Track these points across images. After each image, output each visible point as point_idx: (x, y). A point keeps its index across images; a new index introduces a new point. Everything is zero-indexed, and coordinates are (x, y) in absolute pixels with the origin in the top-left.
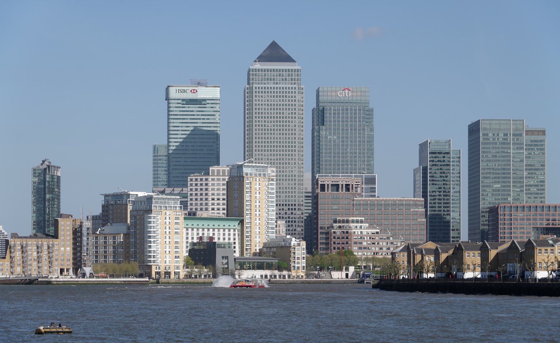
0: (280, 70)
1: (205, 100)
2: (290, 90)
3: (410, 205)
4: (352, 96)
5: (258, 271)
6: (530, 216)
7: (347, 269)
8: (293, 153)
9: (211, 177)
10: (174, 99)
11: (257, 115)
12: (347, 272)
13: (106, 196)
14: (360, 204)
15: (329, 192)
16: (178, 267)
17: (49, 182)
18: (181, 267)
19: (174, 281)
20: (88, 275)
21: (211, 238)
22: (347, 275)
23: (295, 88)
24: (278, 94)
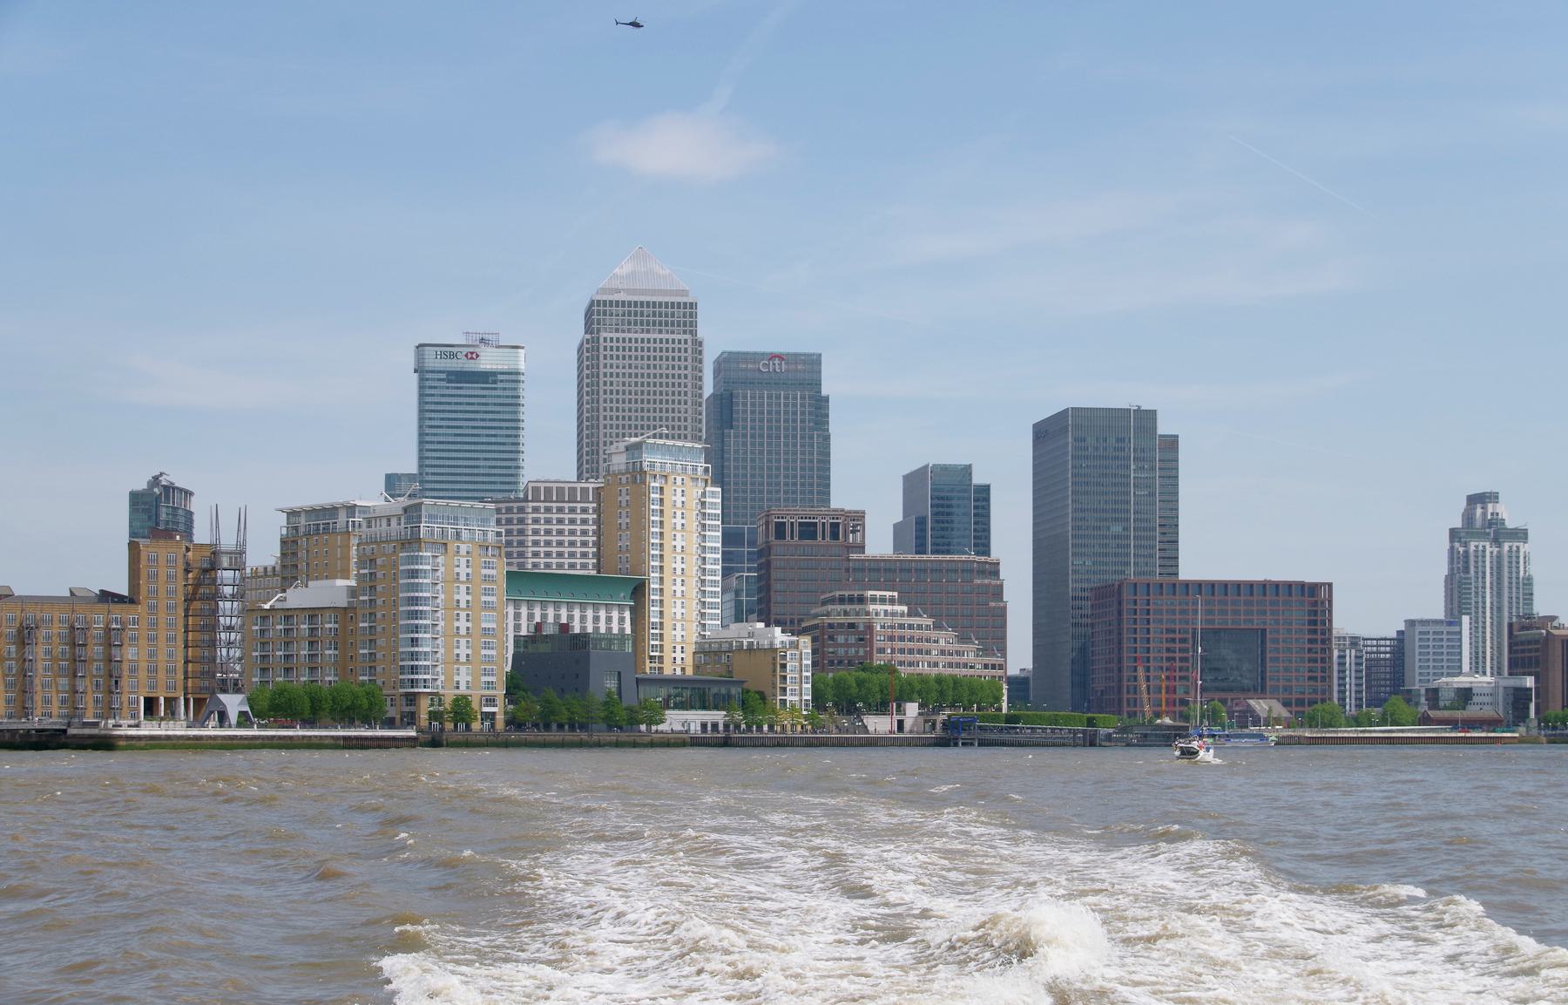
1: (494, 374)
3: (971, 571)
7: (900, 710)
13: (292, 514)
14: (863, 570)
16: (491, 701)
18: (500, 701)
19: (483, 739)
20: (233, 717)
21: (565, 628)
22: (901, 723)
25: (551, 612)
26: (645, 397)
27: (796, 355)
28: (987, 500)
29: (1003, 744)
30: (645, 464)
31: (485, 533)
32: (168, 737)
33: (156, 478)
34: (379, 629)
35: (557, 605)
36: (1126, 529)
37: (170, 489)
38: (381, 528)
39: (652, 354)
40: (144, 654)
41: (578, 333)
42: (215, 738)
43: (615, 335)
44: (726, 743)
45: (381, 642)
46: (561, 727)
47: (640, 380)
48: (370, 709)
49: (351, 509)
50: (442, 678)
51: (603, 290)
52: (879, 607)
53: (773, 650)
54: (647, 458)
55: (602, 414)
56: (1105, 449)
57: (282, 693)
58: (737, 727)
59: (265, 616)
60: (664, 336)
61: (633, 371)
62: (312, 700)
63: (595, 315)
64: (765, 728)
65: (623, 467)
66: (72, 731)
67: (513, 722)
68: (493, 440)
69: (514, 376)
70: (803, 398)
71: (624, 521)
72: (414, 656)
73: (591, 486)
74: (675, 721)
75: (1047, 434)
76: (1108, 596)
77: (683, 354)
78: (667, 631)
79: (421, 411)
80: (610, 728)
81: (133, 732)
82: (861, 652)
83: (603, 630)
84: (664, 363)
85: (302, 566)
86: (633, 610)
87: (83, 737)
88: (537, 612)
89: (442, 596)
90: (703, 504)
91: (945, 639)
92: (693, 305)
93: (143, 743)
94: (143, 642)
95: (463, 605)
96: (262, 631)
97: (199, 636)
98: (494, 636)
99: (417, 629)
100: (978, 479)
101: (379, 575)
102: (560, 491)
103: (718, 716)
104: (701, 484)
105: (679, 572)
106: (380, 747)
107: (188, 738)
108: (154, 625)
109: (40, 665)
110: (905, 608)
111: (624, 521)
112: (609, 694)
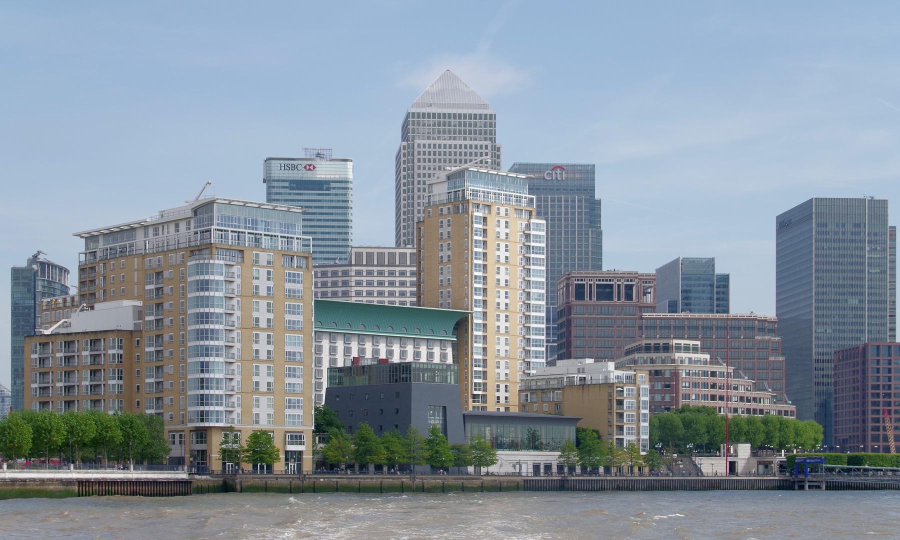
0: (465, 115)
1: (328, 182)
3: (753, 328)
4: (567, 179)
9: (354, 268)
10: (278, 181)
13: (91, 238)
15: (592, 301)
16: (297, 438)
18: (308, 438)
19: (285, 482)
22: (732, 467)
23: (486, 147)
25: (369, 346)
27: (574, 166)
28: (726, 286)
29: (866, 487)
30: (467, 193)
33: (35, 257)
34: (166, 353)
36: (861, 301)
41: (395, 142)
43: (427, 142)
44: (562, 486)
45: (169, 369)
46: (379, 468)
50: (238, 410)
51: (418, 105)
54: (470, 187)
56: (844, 233)
58: (572, 469)
60: (468, 142)
62: (38, 430)
64: (601, 470)
65: (444, 198)
67: (324, 464)
68: (327, 236)
70: (580, 201)
71: (445, 253)
73: (408, 251)
74: (508, 462)
75: (789, 224)
80: (434, 469)
82: (667, 398)
88: (354, 346)
89: (238, 313)
90: (528, 236)
95: (263, 324)
96: (42, 361)
99: (207, 351)
100: (719, 270)
101: (167, 290)
102: (381, 256)
103: (552, 457)
104: (525, 216)
105: (502, 307)
110: (708, 357)
111: (445, 253)
112: (434, 431)
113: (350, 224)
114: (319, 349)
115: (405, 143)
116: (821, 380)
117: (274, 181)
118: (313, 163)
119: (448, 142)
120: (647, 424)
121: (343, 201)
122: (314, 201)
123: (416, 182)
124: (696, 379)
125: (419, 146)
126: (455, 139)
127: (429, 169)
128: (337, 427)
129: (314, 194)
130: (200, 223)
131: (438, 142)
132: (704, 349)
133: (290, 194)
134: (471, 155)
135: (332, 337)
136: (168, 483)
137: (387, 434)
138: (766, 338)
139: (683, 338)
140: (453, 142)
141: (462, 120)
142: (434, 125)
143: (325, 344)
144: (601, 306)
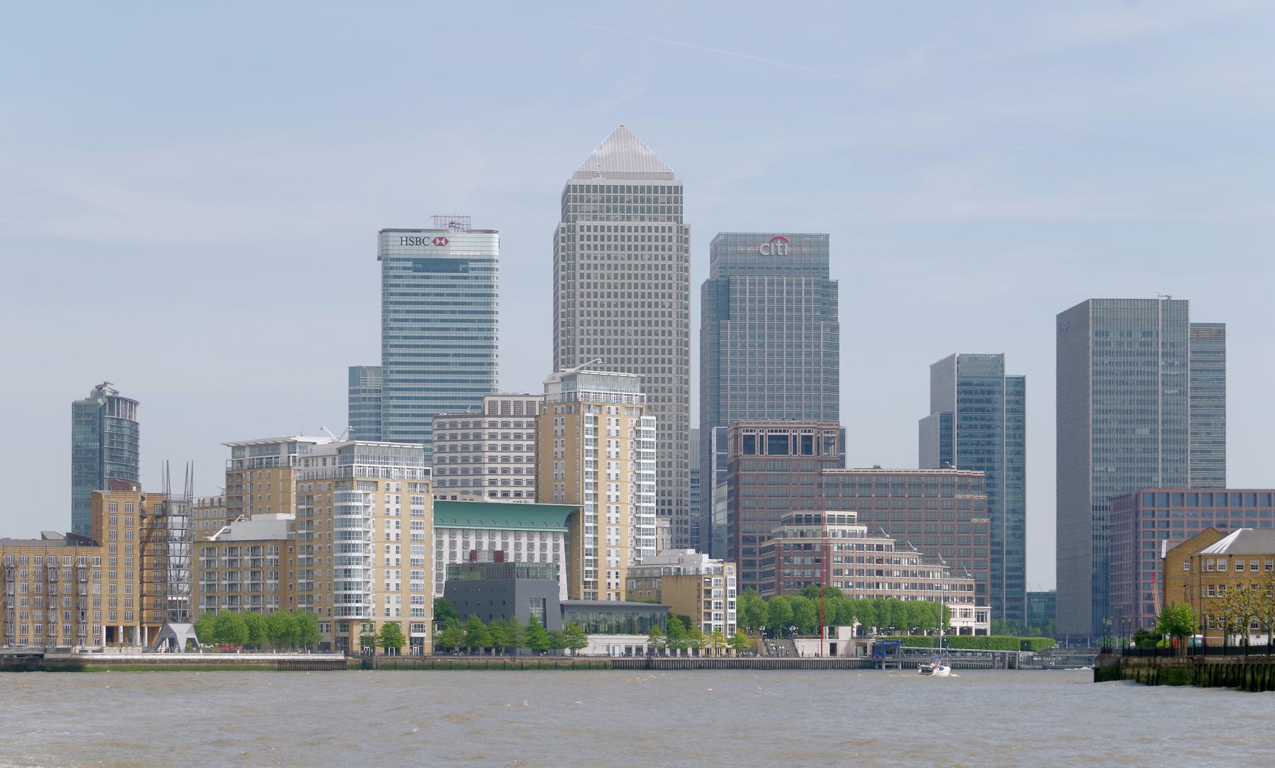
0: (642, 188)
1: (465, 261)
2: (660, 234)
3: (952, 485)
4: (791, 254)
5: (619, 636)
6: (1211, 515)
7: (832, 633)
8: (667, 375)
9: (488, 419)
11: (585, 300)
12: (833, 641)
13: (237, 448)
15: (762, 455)
16: (419, 627)
17: (111, 435)
18: (428, 627)
19: (410, 662)
20: (182, 643)
21: (499, 556)
22: (833, 648)
23: (670, 229)
24: (606, 290)
25: (485, 540)
26: (626, 290)
30: (579, 395)
31: (414, 472)
32: (127, 661)
33: (99, 388)
34: (316, 561)
35: (492, 533)
37: (114, 400)
38: (317, 468)
39: (633, 243)
40: (106, 590)
41: (553, 219)
42: (167, 661)
43: (592, 223)
44: (648, 666)
45: (318, 572)
46: (488, 651)
47: (619, 272)
48: (303, 635)
49: (292, 445)
51: (579, 174)
52: (837, 528)
53: (698, 576)
55: (579, 309)
56: (1130, 344)
57: (226, 620)
58: (662, 651)
59: (211, 548)
60: (646, 224)
61: (613, 262)
63: (573, 198)
64: (690, 651)
65: (559, 398)
66: (48, 656)
67: (441, 648)
68: (464, 334)
69: (487, 264)
71: (560, 449)
72: (347, 586)
74: (597, 645)
75: (1073, 325)
76: (1125, 506)
77: (667, 243)
78: (601, 557)
79: (385, 303)
81: (98, 656)
82: (818, 574)
83: (537, 559)
84: (646, 252)
85: (247, 498)
86: (566, 536)
87: (57, 660)
88: (472, 541)
90: (638, 432)
91: (908, 559)
92: (678, 189)
93: (107, 666)
94: (105, 580)
96: (209, 562)
97: (152, 573)
98: (422, 566)
100: (1011, 370)
101: (316, 510)
103: (641, 640)
104: (636, 412)
105: (613, 499)
106: (311, 669)
107: (144, 661)
108: (114, 564)
109: (18, 599)
110: (865, 529)
113: (495, 317)
114: (440, 544)
115: (564, 225)
116: (1101, 532)
117: (392, 260)
118: (446, 235)
119: (620, 224)
120: (734, 611)
121: (486, 286)
122: (446, 286)
123: (578, 275)
124: (848, 553)
125: (582, 228)
126: (629, 219)
127: (595, 258)
128: (454, 617)
129: (447, 277)
130: (343, 460)
131: (606, 223)
132: (861, 521)
133: (414, 277)
134: (589, 352)
135: (452, 532)
136: (331, 662)
137: (493, 622)
138: (968, 496)
139: (837, 509)
140: (626, 224)
141: (639, 195)
142: (602, 201)
143: (446, 539)
144: (774, 460)
